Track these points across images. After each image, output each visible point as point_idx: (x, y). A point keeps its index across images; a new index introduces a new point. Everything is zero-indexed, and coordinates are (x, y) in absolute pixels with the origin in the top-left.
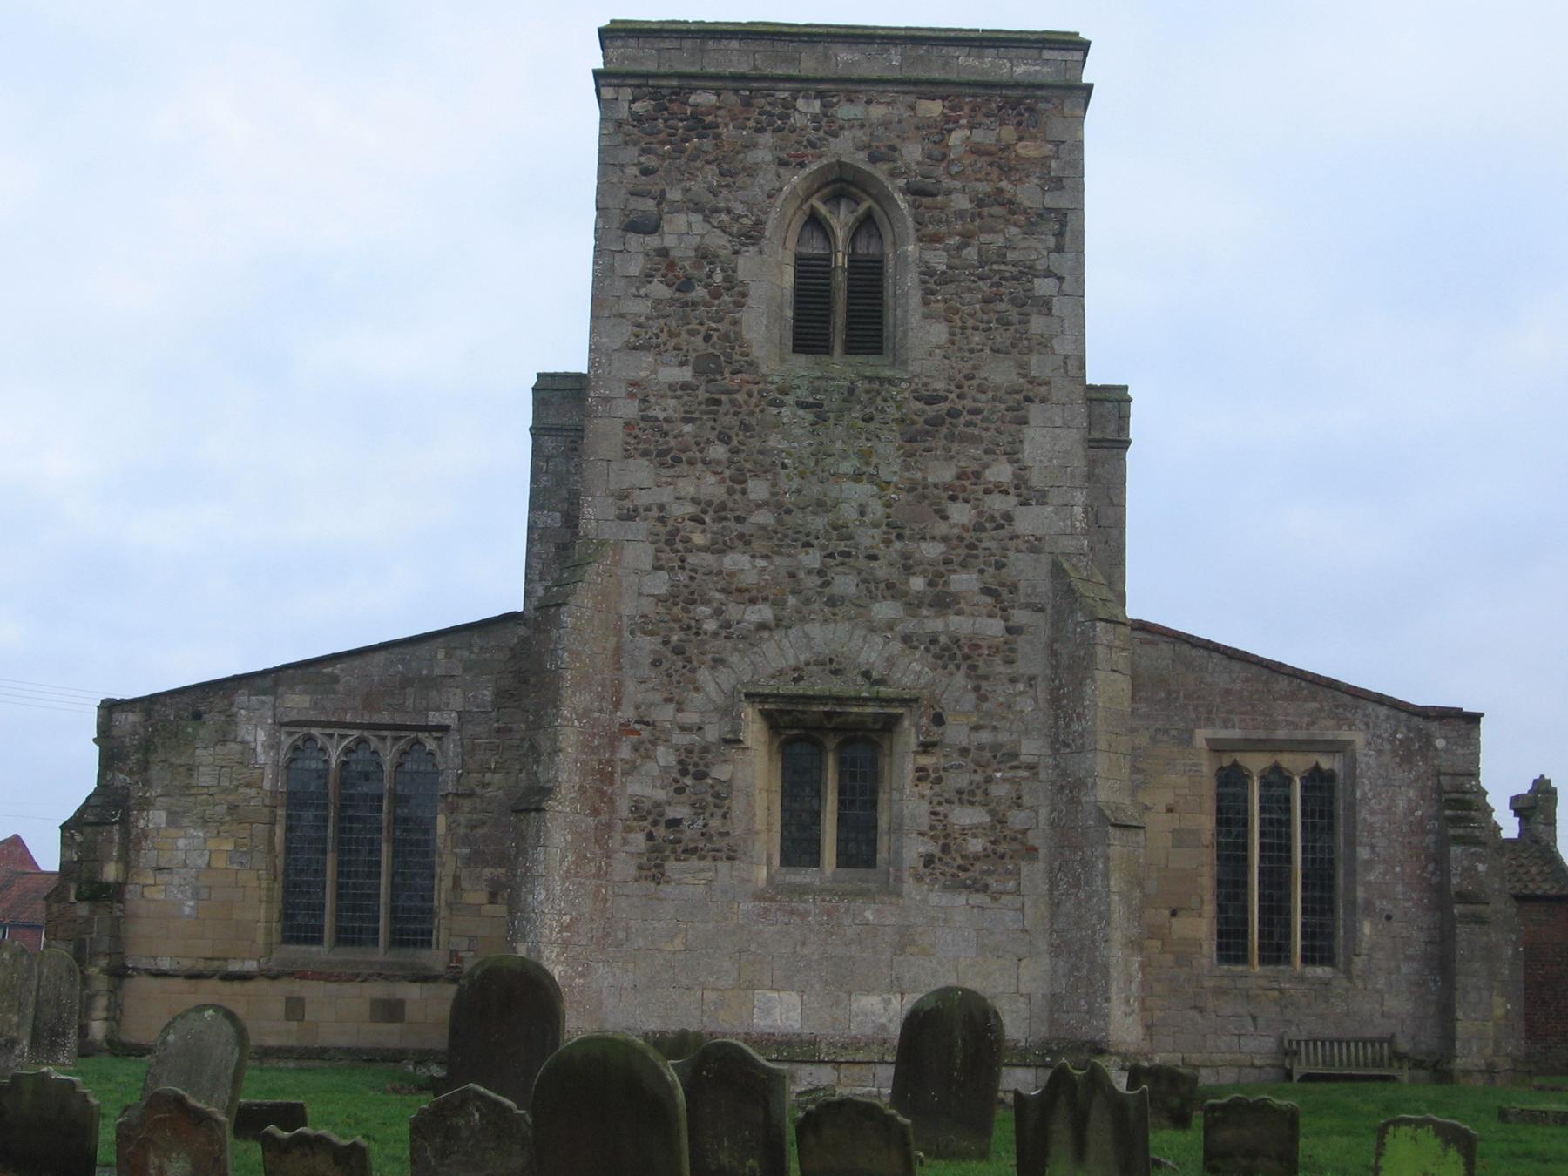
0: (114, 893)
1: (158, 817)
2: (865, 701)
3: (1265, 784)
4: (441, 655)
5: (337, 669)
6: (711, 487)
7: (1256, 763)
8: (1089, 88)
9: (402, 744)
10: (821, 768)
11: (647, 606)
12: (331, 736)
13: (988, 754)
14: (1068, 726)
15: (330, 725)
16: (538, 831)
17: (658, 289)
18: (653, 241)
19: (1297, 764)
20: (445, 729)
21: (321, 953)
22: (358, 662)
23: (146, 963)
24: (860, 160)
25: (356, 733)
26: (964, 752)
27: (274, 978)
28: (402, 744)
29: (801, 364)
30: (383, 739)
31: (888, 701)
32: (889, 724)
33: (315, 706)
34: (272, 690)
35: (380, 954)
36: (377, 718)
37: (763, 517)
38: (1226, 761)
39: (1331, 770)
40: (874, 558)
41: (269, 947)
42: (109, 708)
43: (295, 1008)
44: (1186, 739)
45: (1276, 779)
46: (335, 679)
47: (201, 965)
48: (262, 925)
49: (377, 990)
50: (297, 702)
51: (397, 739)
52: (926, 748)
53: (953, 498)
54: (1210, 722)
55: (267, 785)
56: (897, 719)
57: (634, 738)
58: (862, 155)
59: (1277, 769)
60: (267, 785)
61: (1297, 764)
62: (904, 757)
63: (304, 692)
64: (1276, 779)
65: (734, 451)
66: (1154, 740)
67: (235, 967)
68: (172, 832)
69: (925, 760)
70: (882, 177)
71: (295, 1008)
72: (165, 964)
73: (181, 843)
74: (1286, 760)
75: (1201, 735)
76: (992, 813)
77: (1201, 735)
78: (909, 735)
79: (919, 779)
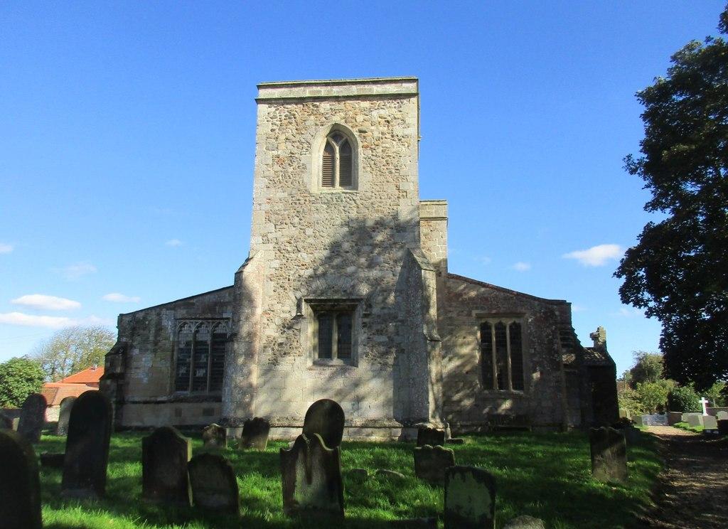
0: (122, 376)
1: (136, 351)
2: (345, 301)
3: (497, 328)
4: (227, 295)
5: (195, 301)
6: (294, 232)
7: (493, 322)
8: (674, 58)
9: (214, 324)
10: (332, 324)
11: (273, 271)
12: (192, 323)
13: (387, 317)
14: (414, 306)
15: (192, 319)
16: (549, 445)
17: (277, 168)
18: (275, 153)
19: (508, 322)
20: (228, 319)
21: (188, 393)
22: (200, 298)
23: (131, 399)
24: (342, 122)
25: (200, 321)
26: (379, 316)
27: (173, 402)
28: (214, 324)
29: (326, 190)
30: (209, 323)
31: (353, 300)
32: (353, 308)
33: (187, 313)
34: (174, 309)
35: (207, 393)
36: (207, 316)
37: (311, 240)
38: (483, 321)
39: (519, 323)
40: (347, 252)
41: (171, 393)
42: (121, 316)
43: (178, 413)
44: (469, 315)
45: (500, 328)
46: (193, 304)
47: (148, 399)
48: (168, 385)
49: (205, 405)
50: (182, 312)
51: (213, 323)
52: (366, 316)
53: (374, 231)
54: (477, 308)
55: (171, 339)
56: (356, 305)
57: (268, 316)
58: (343, 121)
59: (500, 323)
60: (171, 339)
61: (508, 322)
62: (358, 320)
63: (185, 308)
64: (500, 328)
65: (301, 220)
66: (458, 315)
67: (159, 399)
68: (140, 356)
69: (366, 320)
70: (350, 128)
71: (178, 413)
72: (137, 399)
73: (144, 359)
74: (504, 321)
75: (474, 313)
76: (389, 337)
77: (474, 313)
78: (360, 311)
79: (364, 327)
